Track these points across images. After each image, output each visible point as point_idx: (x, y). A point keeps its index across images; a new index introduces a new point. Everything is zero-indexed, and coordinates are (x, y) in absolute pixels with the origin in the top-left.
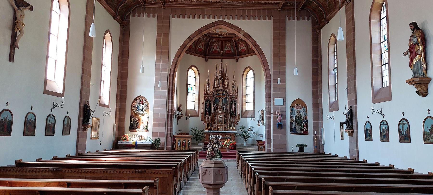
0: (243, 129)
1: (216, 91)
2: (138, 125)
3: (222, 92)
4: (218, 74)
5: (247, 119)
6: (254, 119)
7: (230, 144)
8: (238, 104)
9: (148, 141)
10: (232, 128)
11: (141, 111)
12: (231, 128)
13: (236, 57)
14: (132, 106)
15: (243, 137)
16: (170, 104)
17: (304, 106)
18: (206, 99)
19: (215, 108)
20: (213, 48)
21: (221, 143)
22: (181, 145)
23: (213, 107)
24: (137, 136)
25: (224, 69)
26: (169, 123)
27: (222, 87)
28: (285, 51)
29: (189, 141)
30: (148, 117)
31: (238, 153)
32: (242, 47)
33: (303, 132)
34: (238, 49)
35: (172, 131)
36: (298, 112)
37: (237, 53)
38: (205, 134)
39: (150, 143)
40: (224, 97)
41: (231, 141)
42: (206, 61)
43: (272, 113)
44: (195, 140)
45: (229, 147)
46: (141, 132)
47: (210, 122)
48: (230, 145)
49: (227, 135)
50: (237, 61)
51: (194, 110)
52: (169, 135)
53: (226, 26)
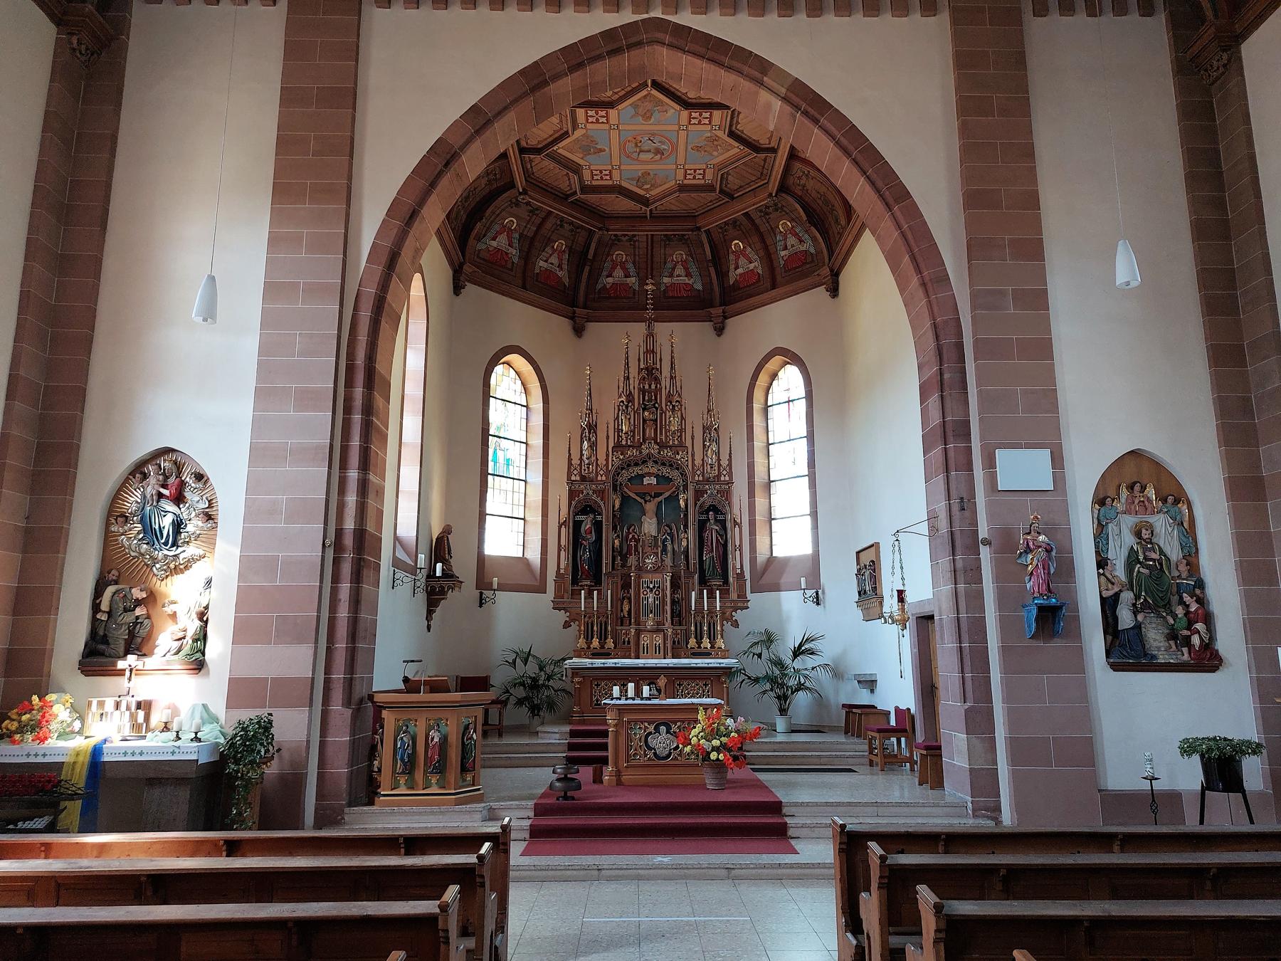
1: (628, 465)
2: (143, 633)
3: (654, 470)
4: (634, 383)
7: (724, 739)
10: (709, 646)
11: (166, 544)
12: (706, 643)
13: (712, 310)
14: (114, 514)
15: (772, 690)
16: (351, 499)
17: (1173, 496)
18: (579, 502)
20: (610, 276)
21: (668, 732)
22: (413, 757)
23: (614, 543)
24: (117, 706)
25: (661, 360)
26: (343, 613)
27: (656, 443)
28: (1031, 174)
29: (467, 728)
30: (209, 583)
32: (742, 261)
33: (1190, 653)
34: (722, 275)
36: (1145, 534)
37: (718, 294)
38: (573, 677)
39: (188, 751)
40: (667, 494)
41: (729, 721)
42: (579, 331)
43: (986, 542)
44: (525, 710)
45: (721, 757)
46: (160, 677)
47: (598, 618)
48: (729, 750)
49: (603, 680)
50: (720, 331)
51: (523, 561)
52: (338, 695)
53: (684, 52)
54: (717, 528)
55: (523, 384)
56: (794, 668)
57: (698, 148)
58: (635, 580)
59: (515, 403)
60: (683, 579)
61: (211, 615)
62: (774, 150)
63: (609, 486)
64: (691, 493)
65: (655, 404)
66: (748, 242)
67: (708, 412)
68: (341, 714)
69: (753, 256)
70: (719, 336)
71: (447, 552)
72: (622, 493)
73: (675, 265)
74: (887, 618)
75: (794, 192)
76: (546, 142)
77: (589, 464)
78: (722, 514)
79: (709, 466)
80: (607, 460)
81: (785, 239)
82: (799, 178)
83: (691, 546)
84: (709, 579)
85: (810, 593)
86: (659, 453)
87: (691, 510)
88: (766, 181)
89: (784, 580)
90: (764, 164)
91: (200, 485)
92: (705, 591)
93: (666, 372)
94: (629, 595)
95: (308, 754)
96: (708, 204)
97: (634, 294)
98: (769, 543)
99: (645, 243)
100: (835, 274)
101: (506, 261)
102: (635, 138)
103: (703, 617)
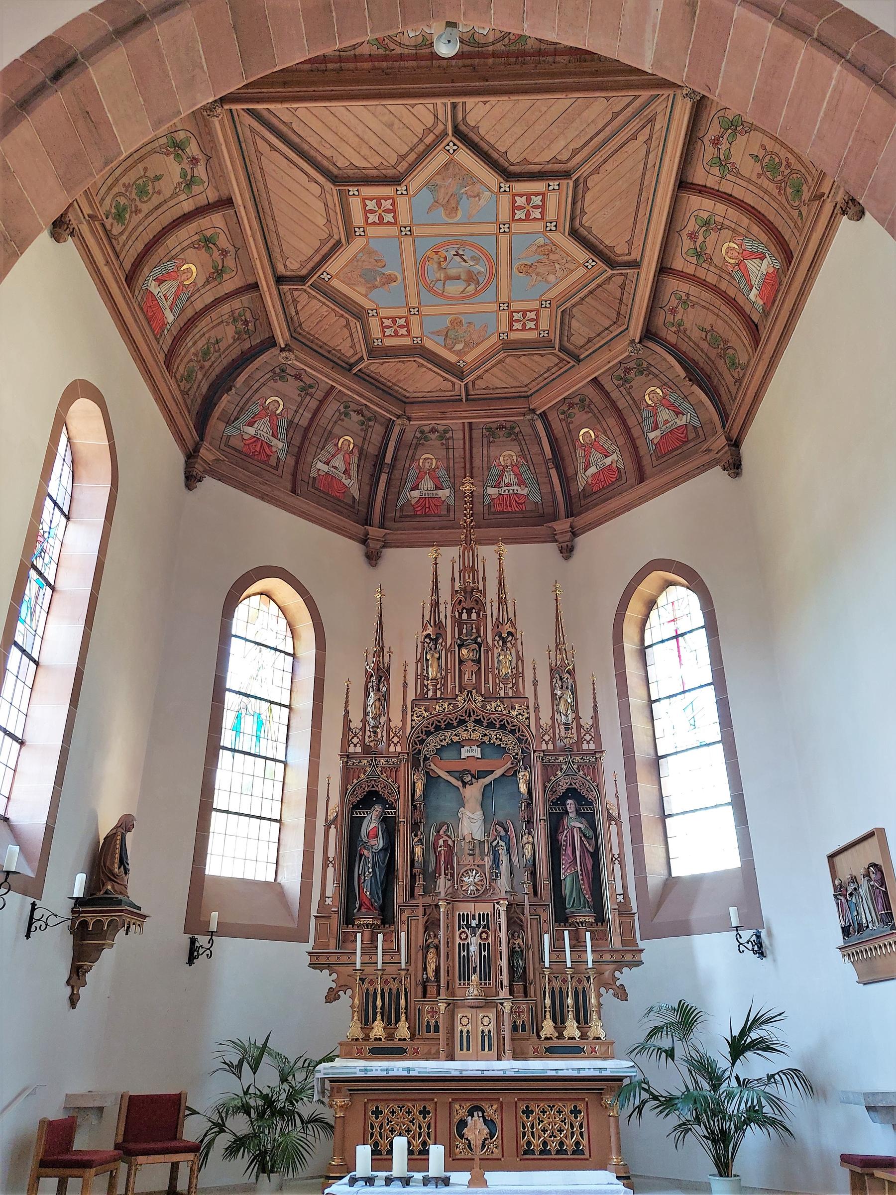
3: (476, 735)
4: (446, 611)
5: (690, 955)
8: (610, 817)
10: (577, 1034)
12: (572, 1028)
15: (698, 1120)
20: (415, 488)
23: (413, 852)
25: (484, 579)
32: (595, 456)
34: (566, 480)
50: (567, 551)
51: (275, 888)
54: (581, 826)
55: (289, 624)
56: (737, 1078)
57: (527, 269)
59: (276, 649)
62: (636, 264)
64: (537, 766)
65: (476, 638)
66: (602, 427)
67: (557, 646)
69: (609, 446)
70: (567, 558)
71: (117, 861)
72: (427, 773)
73: (503, 471)
75: (665, 340)
76: (311, 264)
80: (404, 720)
81: (655, 415)
82: (673, 311)
84: (573, 912)
85: (747, 935)
86: (484, 706)
87: (538, 794)
88: (625, 327)
89: (696, 915)
90: (622, 294)
92: (566, 933)
93: (492, 593)
94: (436, 941)
96: (545, 375)
97: (448, 510)
98: (664, 855)
99: (462, 442)
100: (735, 444)
101: (268, 456)
102: (437, 253)
103: (565, 981)
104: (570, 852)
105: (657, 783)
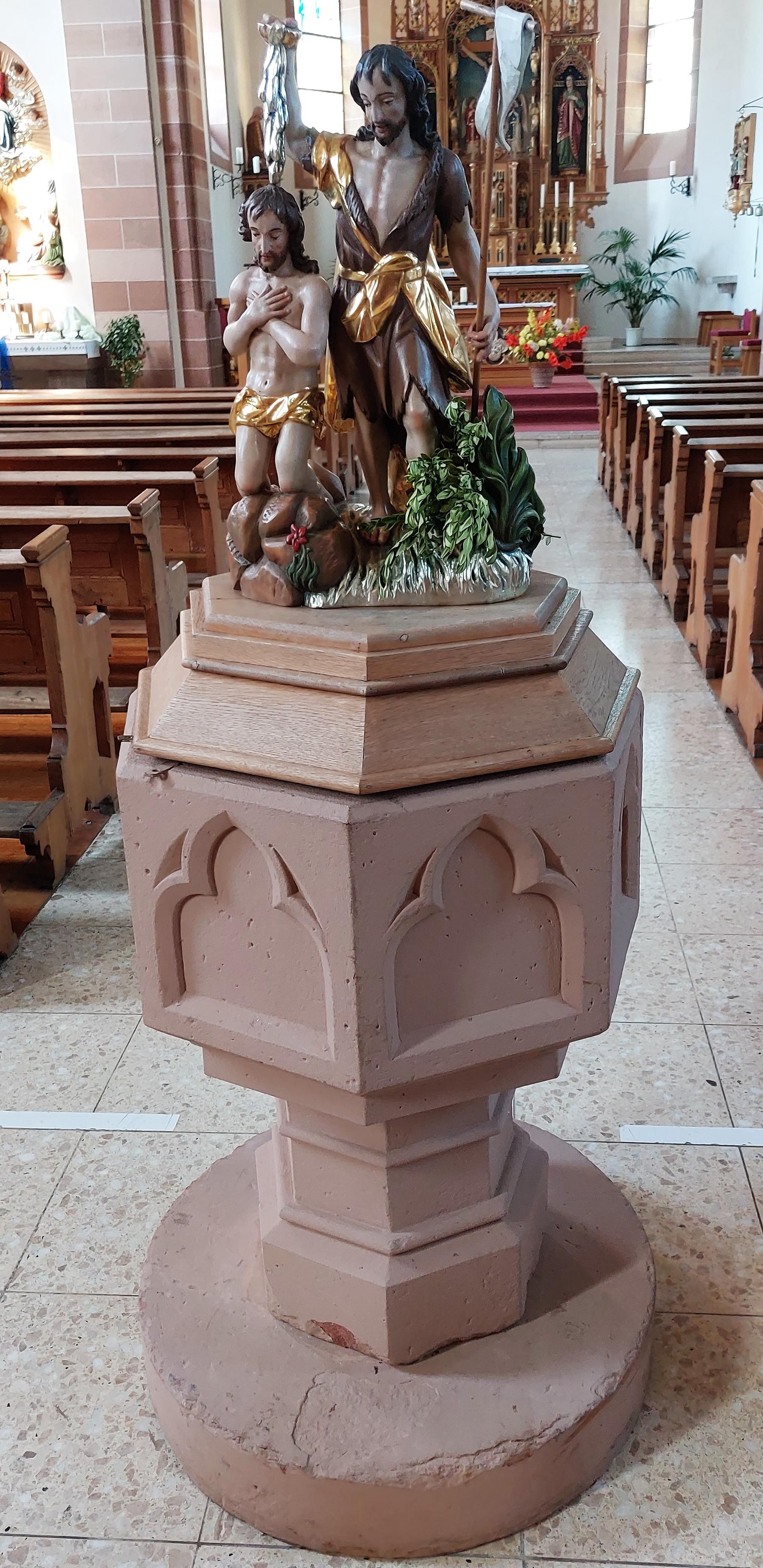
0: (624, 251)
6: (688, 187)
8: (598, 90)
9: (70, 335)
10: (558, 250)
12: (556, 247)
15: (625, 299)
16: (172, 89)
19: (459, 128)
21: (500, 337)
26: (182, 216)
31: (624, 395)
35: (204, 273)
39: (78, 348)
41: (557, 322)
45: (547, 356)
52: (190, 297)
58: (476, 173)
60: (531, 168)
61: (61, 218)
63: (442, 46)
68: (195, 316)
72: (459, 54)
74: (755, 208)
77: (417, 14)
78: (583, 79)
79: (569, 10)
83: (543, 124)
89: (653, 166)
91: (21, 78)
95: (172, 354)
103: (553, 216)
104: (565, 120)
105: (644, 51)
